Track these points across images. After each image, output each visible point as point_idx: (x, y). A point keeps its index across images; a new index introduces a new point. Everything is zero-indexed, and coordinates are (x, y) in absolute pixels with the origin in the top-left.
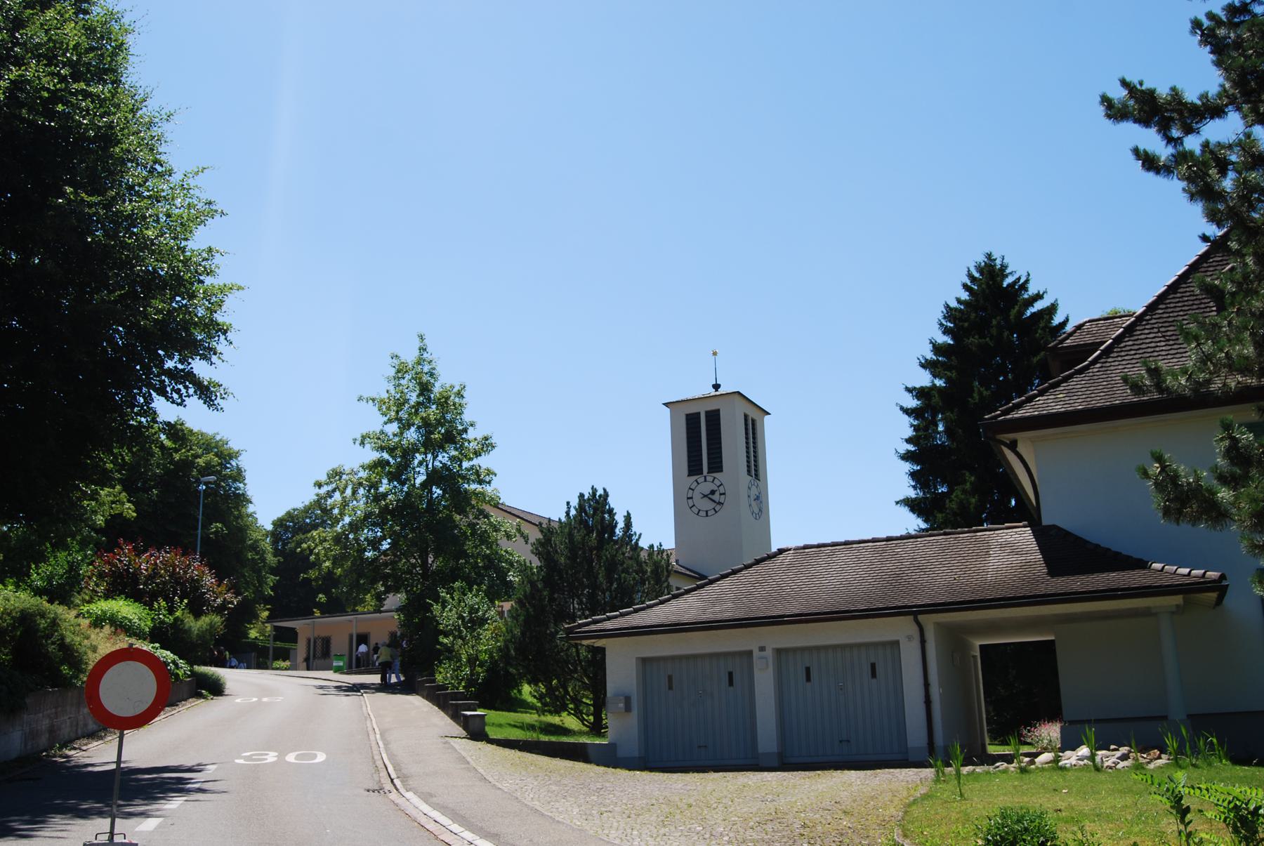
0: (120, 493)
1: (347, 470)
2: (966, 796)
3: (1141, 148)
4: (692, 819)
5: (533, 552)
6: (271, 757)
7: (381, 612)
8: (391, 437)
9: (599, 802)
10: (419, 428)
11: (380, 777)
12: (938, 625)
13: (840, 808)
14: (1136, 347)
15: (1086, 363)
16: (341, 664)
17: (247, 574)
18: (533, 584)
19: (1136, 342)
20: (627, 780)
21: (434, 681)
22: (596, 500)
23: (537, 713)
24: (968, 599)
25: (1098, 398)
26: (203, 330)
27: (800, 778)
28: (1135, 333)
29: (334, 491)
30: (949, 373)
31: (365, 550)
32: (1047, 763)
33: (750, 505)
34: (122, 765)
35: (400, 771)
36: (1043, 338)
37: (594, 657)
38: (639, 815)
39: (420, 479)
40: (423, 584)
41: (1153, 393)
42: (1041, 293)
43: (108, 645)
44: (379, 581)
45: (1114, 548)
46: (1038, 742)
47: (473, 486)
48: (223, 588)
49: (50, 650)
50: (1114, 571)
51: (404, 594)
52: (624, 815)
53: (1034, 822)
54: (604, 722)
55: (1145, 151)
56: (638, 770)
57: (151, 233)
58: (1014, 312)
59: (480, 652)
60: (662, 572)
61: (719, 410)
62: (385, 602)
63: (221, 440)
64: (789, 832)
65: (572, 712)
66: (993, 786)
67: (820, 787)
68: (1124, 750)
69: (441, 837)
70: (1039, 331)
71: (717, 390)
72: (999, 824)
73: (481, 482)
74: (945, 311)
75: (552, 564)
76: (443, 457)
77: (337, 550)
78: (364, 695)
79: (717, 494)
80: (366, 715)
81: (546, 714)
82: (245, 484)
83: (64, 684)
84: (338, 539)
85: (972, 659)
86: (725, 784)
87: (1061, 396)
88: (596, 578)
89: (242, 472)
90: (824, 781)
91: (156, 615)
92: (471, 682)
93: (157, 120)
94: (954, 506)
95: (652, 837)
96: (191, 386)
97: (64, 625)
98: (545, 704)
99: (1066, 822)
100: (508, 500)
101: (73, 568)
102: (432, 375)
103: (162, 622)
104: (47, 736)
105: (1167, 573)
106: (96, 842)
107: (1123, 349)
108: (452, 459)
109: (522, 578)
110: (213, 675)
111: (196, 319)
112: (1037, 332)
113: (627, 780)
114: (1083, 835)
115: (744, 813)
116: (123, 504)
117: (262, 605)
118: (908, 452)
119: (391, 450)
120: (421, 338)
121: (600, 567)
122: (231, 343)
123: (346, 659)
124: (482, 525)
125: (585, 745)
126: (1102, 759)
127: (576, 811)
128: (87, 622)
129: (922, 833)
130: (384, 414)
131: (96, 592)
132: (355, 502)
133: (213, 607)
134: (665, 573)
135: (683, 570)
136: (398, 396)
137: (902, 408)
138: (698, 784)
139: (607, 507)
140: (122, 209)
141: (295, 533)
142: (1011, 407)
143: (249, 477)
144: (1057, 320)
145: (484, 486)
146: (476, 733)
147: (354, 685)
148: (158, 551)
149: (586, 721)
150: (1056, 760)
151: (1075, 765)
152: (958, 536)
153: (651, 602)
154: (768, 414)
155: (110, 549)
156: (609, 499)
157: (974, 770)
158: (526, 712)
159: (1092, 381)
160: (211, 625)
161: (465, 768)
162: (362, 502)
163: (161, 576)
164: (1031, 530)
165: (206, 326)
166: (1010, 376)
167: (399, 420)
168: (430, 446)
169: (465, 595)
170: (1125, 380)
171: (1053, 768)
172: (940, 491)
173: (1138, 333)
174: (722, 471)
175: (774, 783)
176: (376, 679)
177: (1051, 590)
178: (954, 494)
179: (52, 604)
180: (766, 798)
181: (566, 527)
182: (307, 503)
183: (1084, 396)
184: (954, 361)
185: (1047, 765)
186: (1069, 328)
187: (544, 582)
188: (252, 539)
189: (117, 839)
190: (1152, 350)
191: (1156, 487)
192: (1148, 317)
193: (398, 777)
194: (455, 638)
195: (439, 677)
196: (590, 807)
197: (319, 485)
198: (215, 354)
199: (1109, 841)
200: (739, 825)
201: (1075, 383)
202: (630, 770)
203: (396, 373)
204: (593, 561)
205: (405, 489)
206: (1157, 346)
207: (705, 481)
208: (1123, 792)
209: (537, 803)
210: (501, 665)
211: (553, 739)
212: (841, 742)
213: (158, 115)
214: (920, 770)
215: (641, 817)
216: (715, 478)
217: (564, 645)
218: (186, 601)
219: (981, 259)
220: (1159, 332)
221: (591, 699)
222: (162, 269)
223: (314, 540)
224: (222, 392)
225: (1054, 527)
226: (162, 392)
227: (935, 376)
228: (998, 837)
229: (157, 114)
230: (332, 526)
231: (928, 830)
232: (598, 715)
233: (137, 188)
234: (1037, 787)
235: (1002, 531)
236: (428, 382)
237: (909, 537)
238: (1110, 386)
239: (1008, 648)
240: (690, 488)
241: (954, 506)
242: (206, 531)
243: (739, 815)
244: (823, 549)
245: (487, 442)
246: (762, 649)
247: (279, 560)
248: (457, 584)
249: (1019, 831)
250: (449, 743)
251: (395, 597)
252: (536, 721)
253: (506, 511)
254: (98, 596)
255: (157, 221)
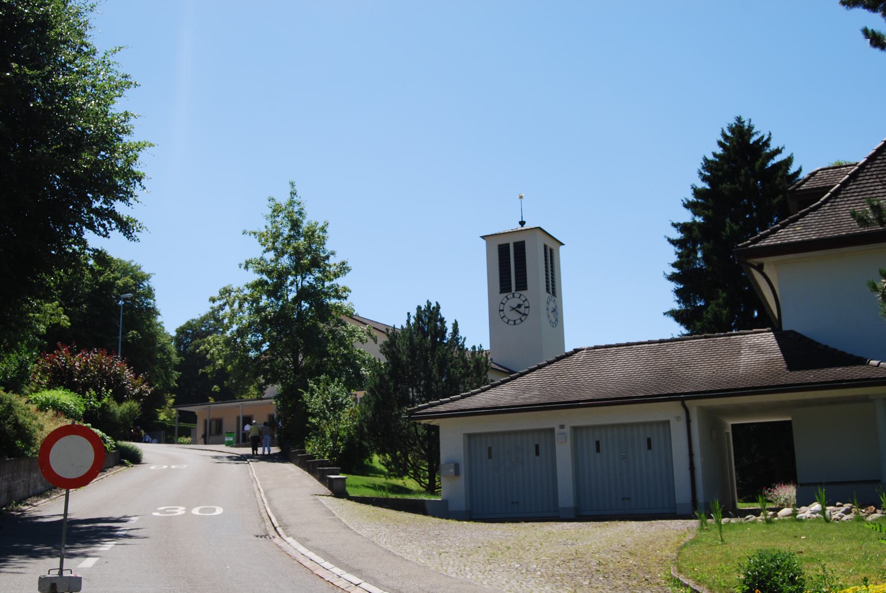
0: (57, 307)
1: (235, 289)
2: (726, 541)
3: (870, 28)
4: (511, 558)
5: (381, 352)
6: (181, 511)
7: (262, 399)
8: (269, 263)
9: (438, 545)
10: (291, 255)
11: (265, 526)
12: (701, 409)
13: (626, 550)
14: (859, 190)
15: (819, 202)
16: (231, 439)
17: (157, 370)
18: (381, 376)
19: (858, 186)
20: (458, 528)
21: (304, 452)
22: (431, 311)
23: (385, 476)
24: (732, 387)
25: (829, 230)
26: (123, 178)
27: (593, 527)
28: (858, 179)
29: (225, 305)
30: (706, 212)
31: (249, 351)
32: (787, 516)
33: (548, 316)
34: (68, 517)
35: (281, 521)
36: (781, 184)
37: (429, 433)
38: (469, 555)
39: (292, 296)
40: (294, 377)
41: (876, 225)
42: (780, 148)
43: (51, 424)
44: (260, 375)
45: (840, 349)
46: (776, 500)
47: (333, 301)
48: (139, 381)
49: (7, 428)
50: (839, 366)
51: (280, 385)
52: (458, 555)
53: (784, 561)
54: (437, 484)
55: (873, 31)
56: (466, 521)
57: (80, 99)
58: (758, 163)
59: (340, 429)
60: (483, 367)
61: (523, 242)
62: (265, 392)
63: (135, 266)
64: (588, 569)
65: (412, 476)
66: (746, 533)
67: (609, 534)
68: (847, 506)
69: (316, 572)
70: (778, 179)
71: (522, 226)
72: (757, 562)
73: (339, 297)
74: (704, 163)
75: (397, 361)
76: (310, 278)
77: (227, 351)
78: (250, 463)
79: (523, 307)
80: (252, 478)
81: (392, 477)
82: (154, 300)
83: (19, 455)
84: (228, 342)
85: (726, 435)
86: (534, 531)
87: (799, 228)
88: (431, 372)
89: (152, 290)
90: (611, 529)
91: (88, 401)
92: (334, 453)
93: (83, 10)
94: (710, 316)
95: (481, 572)
96: (113, 221)
97: (17, 409)
98: (391, 470)
99: (807, 561)
100: (361, 311)
101: (23, 365)
102: (300, 214)
103: (93, 407)
104: (6, 494)
105: (882, 368)
106: (48, 576)
107: (849, 192)
108: (316, 279)
109: (373, 372)
110: (132, 448)
111: (117, 169)
112: (776, 180)
113: (458, 528)
114: (824, 571)
115: (551, 554)
116: (60, 316)
117: (169, 394)
118: (674, 274)
119: (269, 273)
120: (292, 184)
121: (434, 363)
122: (144, 188)
123: (235, 435)
124: (341, 331)
125: (424, 501)
126: (830, 513)
127: (420, 552)
128: (34, 407)
129: (693, 569)
130: (263, 245)
131: (41, 384)
132: (241, 314)
133: (131, 395)
134: (485, 368)
135: (497, 367)
136: (274, 230)
137: (669, 240)
138: (513, 531)
139: (439, 317)
140: (57, 81)
141: (193, 338)
142: (758, 238)
143: (158, 294)
144: (793, 170)
145: (342, 300)
146: (339, 492)
147: (242, 456)
148: (88, 353)
149: (423, 482)
150: (794, 514)
151: (809, 518)
152: (715, 339)
153: (475, 390)
154: (563, 244)
155: (51, 352)
156: (441, 311)
157: (730, 521)
158: (376, 476)
159: (823, 217)
160: (131, 409)
161: (331, 519)
162: (246, 314)
163: (91, 371)
164: (774, 334)
165: (125, 174)
166: (755, 214)
167: (275, 249)
168: (300, 269)
169: (329, 385)
170: (853, 214)
171: (792, 520)
172: (698, 305)
173: (861, 178)
174: (526, 289)
175: (572, 531)
176: (248, 451)
177: (790, 381)
178: (710, 307)
179: (7, 393)
180: (567, 542)
181: (407, 332)
182: (203, 315)
183: (817, 229)
184: (711, 202)
185: (787, 518)
186: (803, 175)
187: (390, 375)
188: (160, 343)
189: (66, 574)
190: (872, 192)
191: (883, 298)
192: (868, 166)
193: (280, 526)
194: (321, 418)
195: (308, 450)
196: (431, 548)
197: (213, 300)
198: (132, 196)
199: (842, 576)
200: (548, 563)
201: (810, 218)
202: (459, 521)
203: (272, 212)
204: (428, 359)
205: (280, 303)
206: (875, 189)
207: (508, 299)
208: (850, 538)
209: (389, 545)
210: (357, 440)
211: (399, 496)
212: (623, 499)
213: (84, 7)
214: (686, 521)
215: (471, 556)
216: (521, 295)
217: (405, 424)
218: (111, 391)
219: (733, 121)
220: (877, 178)
221: (426, 466)
222: (90, 129)
223: (209, 344)
224: (138, 226)
225: (792, 332)
226: (91, 227)
227: (695, 214)
228: (756, 573)
229: (83, 6)
230: (223, 332)
231: (698, 567)
232: (432, 478)
233: (68, 65)
234: (781, 534)
235: (750, 335)
236: (297, 220)
237: (672, 340)
238: (837, 221)
239: (751, 427)
240: (501, 303)
241: (709, 317)
242: (125, 337)
243: (548, 555)
244: (609, 349)
245: (344, 266)
246: (562, 427)
247: (181, 360)
248: (323, 377)
249: (772, 568)
250: (318, 500)
251: (273, 387)
252: (384, 483)
253: (358, 321)
254: (42, 387)
255: (85, 91)
